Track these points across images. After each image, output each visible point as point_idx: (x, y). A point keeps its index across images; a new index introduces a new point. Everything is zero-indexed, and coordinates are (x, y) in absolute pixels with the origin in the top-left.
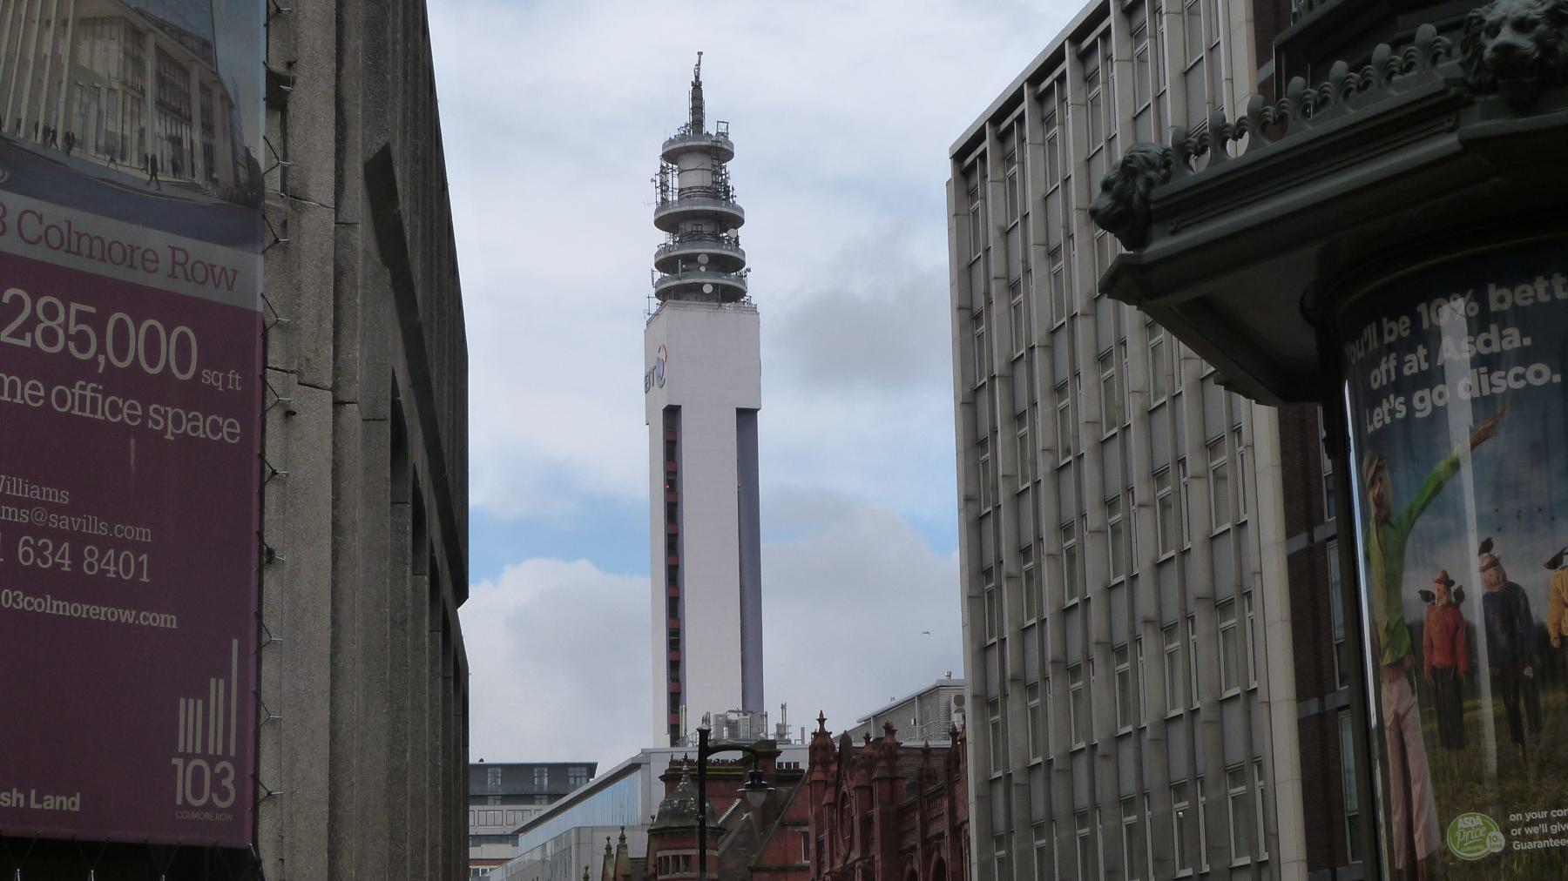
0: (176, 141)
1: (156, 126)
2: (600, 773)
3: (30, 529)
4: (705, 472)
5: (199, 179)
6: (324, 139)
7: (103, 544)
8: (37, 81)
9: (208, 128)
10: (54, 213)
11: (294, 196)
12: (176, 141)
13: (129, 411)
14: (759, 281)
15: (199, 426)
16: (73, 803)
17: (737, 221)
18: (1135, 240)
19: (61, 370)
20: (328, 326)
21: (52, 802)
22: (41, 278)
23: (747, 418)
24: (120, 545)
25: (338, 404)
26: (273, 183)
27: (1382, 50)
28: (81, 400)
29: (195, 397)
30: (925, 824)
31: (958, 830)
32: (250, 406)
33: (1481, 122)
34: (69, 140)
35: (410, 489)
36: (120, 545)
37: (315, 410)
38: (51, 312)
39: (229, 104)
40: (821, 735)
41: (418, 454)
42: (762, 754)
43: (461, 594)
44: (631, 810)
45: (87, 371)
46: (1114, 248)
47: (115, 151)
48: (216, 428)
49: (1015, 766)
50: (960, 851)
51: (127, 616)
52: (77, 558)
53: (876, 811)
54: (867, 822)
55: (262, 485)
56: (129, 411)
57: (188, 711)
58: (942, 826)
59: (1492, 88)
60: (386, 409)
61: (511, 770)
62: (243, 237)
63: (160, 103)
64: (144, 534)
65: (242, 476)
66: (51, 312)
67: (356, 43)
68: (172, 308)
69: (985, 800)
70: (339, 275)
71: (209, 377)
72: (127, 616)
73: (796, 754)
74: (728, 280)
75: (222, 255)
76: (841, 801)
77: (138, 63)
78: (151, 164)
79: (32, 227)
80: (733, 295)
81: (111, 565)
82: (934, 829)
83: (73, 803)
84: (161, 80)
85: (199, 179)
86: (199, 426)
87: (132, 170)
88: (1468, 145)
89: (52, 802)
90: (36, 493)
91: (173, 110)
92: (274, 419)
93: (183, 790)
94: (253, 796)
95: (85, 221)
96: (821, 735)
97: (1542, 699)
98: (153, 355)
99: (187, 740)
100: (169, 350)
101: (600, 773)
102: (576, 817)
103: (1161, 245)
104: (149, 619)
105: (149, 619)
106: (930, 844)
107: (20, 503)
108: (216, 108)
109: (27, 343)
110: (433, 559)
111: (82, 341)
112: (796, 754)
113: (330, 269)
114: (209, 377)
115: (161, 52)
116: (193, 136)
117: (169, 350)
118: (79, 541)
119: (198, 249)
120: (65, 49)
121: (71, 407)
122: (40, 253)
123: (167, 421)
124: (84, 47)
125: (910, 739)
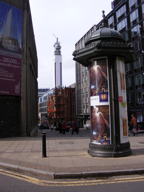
0: (15, 47)
1: (14, 46)
2: (50, 90)
3: (5, 74)
4: (59, 68)
5: (17, 50)
6: (25, 46)
7: (10, 75)
8: (6, 44)
9: (17, 46)
10: (7, 52)
11: (23, 50)
12: (15, 47)
13: (12, 66)
14: (62, 53)
15: (17, 67)
16: (9, 93)
17: (60, 49)
18: (75, 56)
19: (7, 63)
20: (26, 60)
21: (7, 92)
22: (6, 57)
23: (61, 63)
24: (11, 75)
25: (26, 65)
26: (22, 50)
27: (90, 45)
28: (9, 65)
29: (16, 65)
30: (73, 94)
31: (75, 94)
32: (20, 65)
33: (95, 50)
34: (8, 47)
35: (32, 70)
36: (11, 75)
37: (25, 66)
38: (7, 59)
39: (19, 44)
40: (65, 87)
41: (33, 68)
42: (62, 88)
43: (37, 77)
44: (52, 92)
45: (9, 63)
46: (73, 57)
47: (11, 48)
48: (18, 67)
49: (79, 89)
50: (75, 96)
51: (12, 80)
52: (8, 76)
53: (69, 93)
54: (69, 93)
55: (21, 71)
56: (12, 66)
57: (16, 86)
58: (74, 94)
59: (96, 48)
60: (30, 65)
61: (41, 89)
62: (19, 54)
63: (14, 44)
64: (13, 74)
65: (20, 70)
66: (7, 59)
67: (28, 40)
68: (15, 59)
69: (77, 92)
70: (26, 56)
71: (17, 63)
72: (12, 80)
73: (64, 89)
74: (60, 53)
75: (19, 55)
76: (67, 92)
77: (13, 42)
78: (13, 48)
79: (5, 53)
80: (60, 54)
81: (11, 76)
82: (74, 94)
83: (9, 93)
84: (14, 43)
85: (17, 50)
86: (17, 67)
87: (12, 49)
88: (94, 51)
89: (7, 92)
90: (6, 71)
91: (15, 45)
92: (22, 66)
93: (16, 92)
94: (21, 92)
95: (9, 53)
96: (65, 87)
97: (38, 93)
98: (13, 61)
99: (16, 88)
100: (15, 61)
101: (50, 90)
102: (48, 93)
103: (77, 57)
104: (13, 80)
105: (13, 80)
106: (73, 95)
107: (4, 72)
108: (18, 45)
109: (5, 61)
110: (34, 75)
111: (9, 61)
112: (64, 89)
113: (26, 55)
114: (17, 63)
115: (14, 41)
116: (16, 47)
117: (15, 61)
118: (8, 75)
119: (16, 54)
120: (8, 41)
121: (8, 66)
122: (6, 55)
123: (15, 66)
124: (9, 41)
125: (72, 87)
